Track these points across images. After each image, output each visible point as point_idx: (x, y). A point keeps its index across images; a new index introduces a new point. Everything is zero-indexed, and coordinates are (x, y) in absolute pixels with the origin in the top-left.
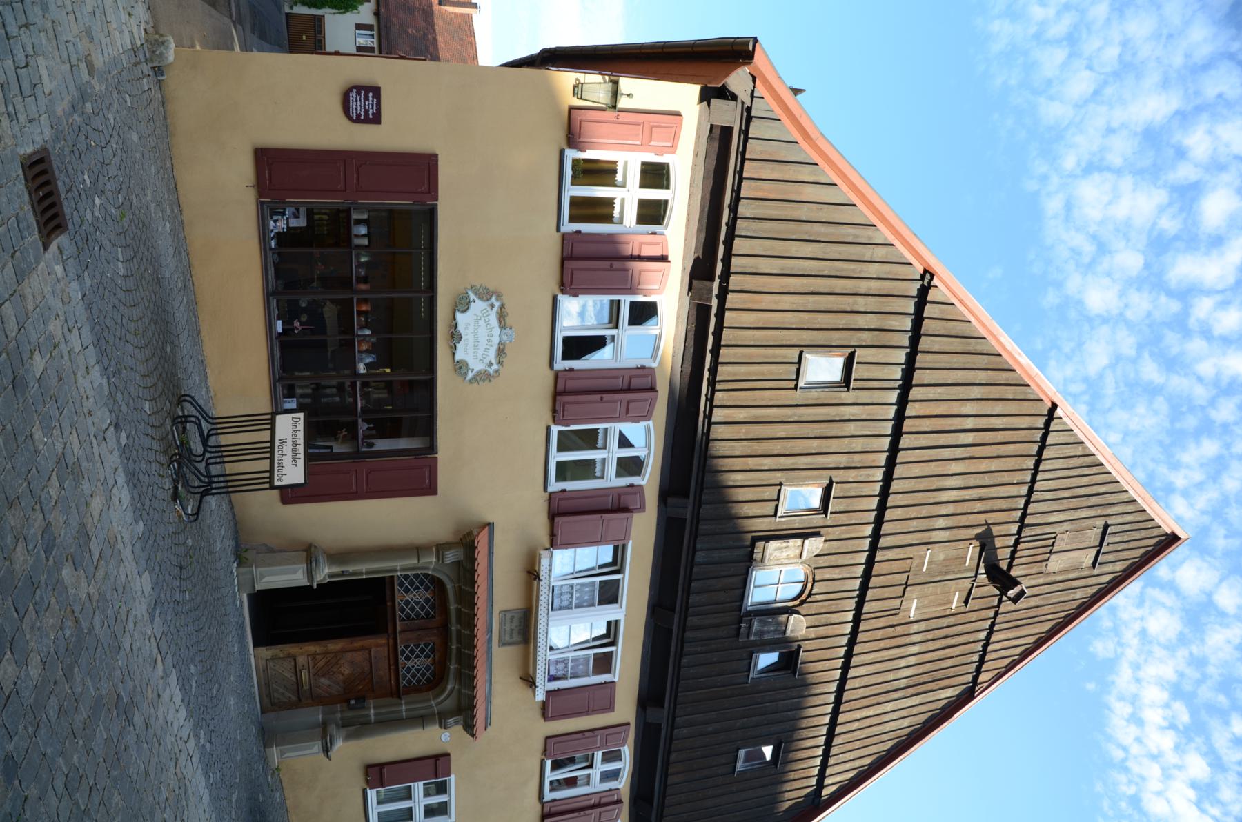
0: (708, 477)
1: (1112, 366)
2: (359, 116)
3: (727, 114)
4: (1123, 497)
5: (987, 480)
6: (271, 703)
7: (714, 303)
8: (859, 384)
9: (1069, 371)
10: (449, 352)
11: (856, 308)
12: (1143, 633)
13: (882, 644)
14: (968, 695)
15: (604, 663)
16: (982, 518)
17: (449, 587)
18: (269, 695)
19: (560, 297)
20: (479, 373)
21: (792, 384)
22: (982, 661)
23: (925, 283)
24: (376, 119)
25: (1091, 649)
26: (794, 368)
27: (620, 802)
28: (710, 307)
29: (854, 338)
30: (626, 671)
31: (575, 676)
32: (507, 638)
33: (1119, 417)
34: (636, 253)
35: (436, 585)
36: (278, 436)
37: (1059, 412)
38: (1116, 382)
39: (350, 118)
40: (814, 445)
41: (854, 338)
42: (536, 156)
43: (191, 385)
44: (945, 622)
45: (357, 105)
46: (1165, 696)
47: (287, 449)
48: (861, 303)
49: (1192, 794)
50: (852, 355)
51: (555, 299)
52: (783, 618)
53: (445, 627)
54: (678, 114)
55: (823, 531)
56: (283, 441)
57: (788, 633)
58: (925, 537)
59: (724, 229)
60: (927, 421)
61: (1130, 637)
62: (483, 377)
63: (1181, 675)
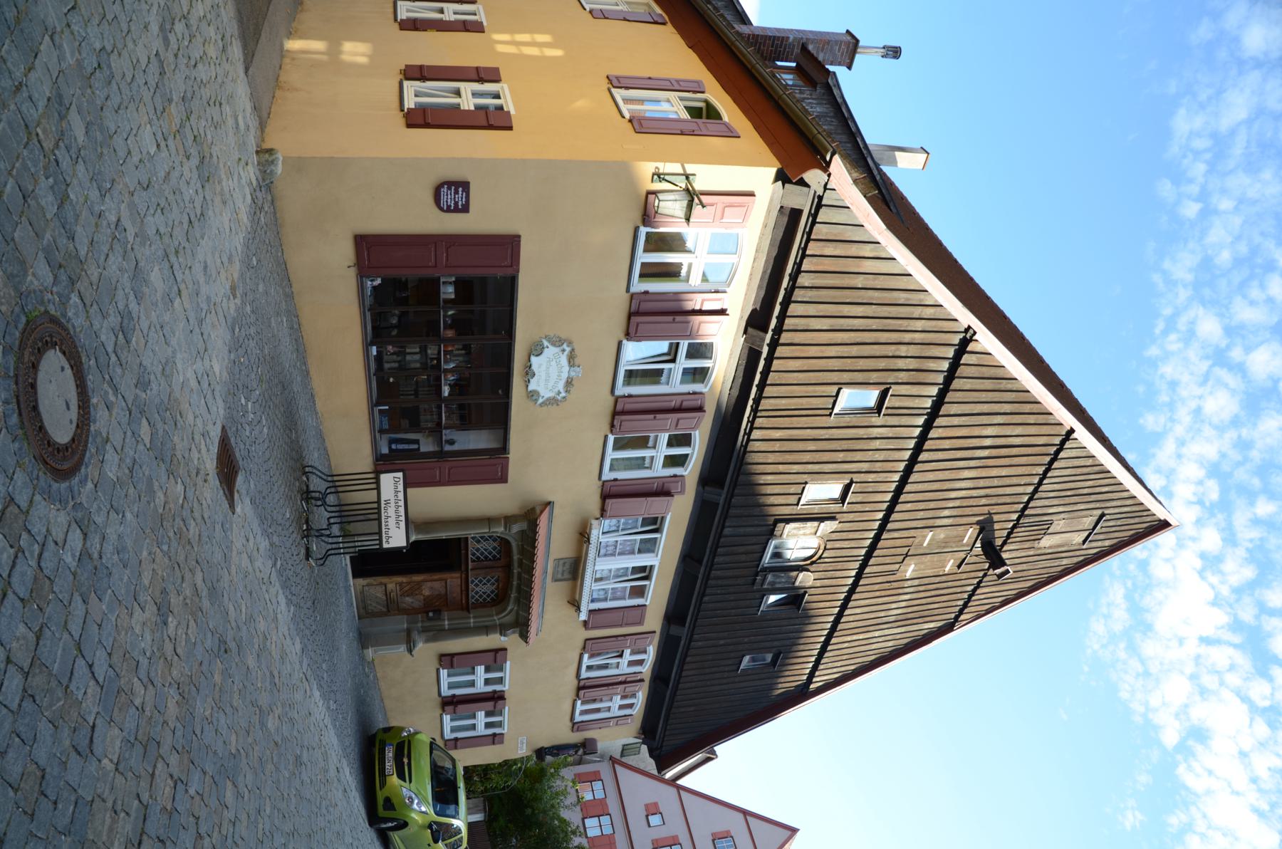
0: (742, 478)
1: (1249, 122)
2: (449, 207)
3: (801, 200)
4: (1125, 495)
5: (996, 482)
6: (365, 613)
7: (765, 350)
8: (890, 411)
9: (1198, 122)
10: (523, 384)
11: (897, 353)
12: (1198, 411)
13: (878, 594)
14: (948, 628)
15: (639, 592)
16: (985, 510)
17: (514, 544)
18: (365, 608)
19: (625, 342)
20: (548, 399)
21: (828, 412)
22: (965, 605)
23: (968, 336)
24: (466, 209)
25: (1141, 421)
26: (832, 400)
27: (642, 680)
28: (760, 353)
29: (891, 377)
30: (657, 596)
31: (614, 599)
32: (559, 576)
33: (1240, 182)
34: (697, 307)
35: (505, 543)
36: (383, 499)
37: (1074, 435)
38: (1248, 142)
39: (441, 209)
40: (841, 456)
41: (891, 377)
42: (613, 234)
43: (313, 458)
44: (938, 579)
45: (448, 197)
46: (1201, 473)
47: (391, 511)
48: (903, 350)
49: (1198, 563)
50: (887, 390)
51: (620, 344)
52: (794, 574)
53: (508, 567)
54: (752, 194)
55: (838, 516)
56: (387, 502)
57: (797, 584)
58: (930, 523)
59: (782, 292)
60: (948, 441)
61: (1184, 415)
62: (552, 401)
63: (1223, 456)
